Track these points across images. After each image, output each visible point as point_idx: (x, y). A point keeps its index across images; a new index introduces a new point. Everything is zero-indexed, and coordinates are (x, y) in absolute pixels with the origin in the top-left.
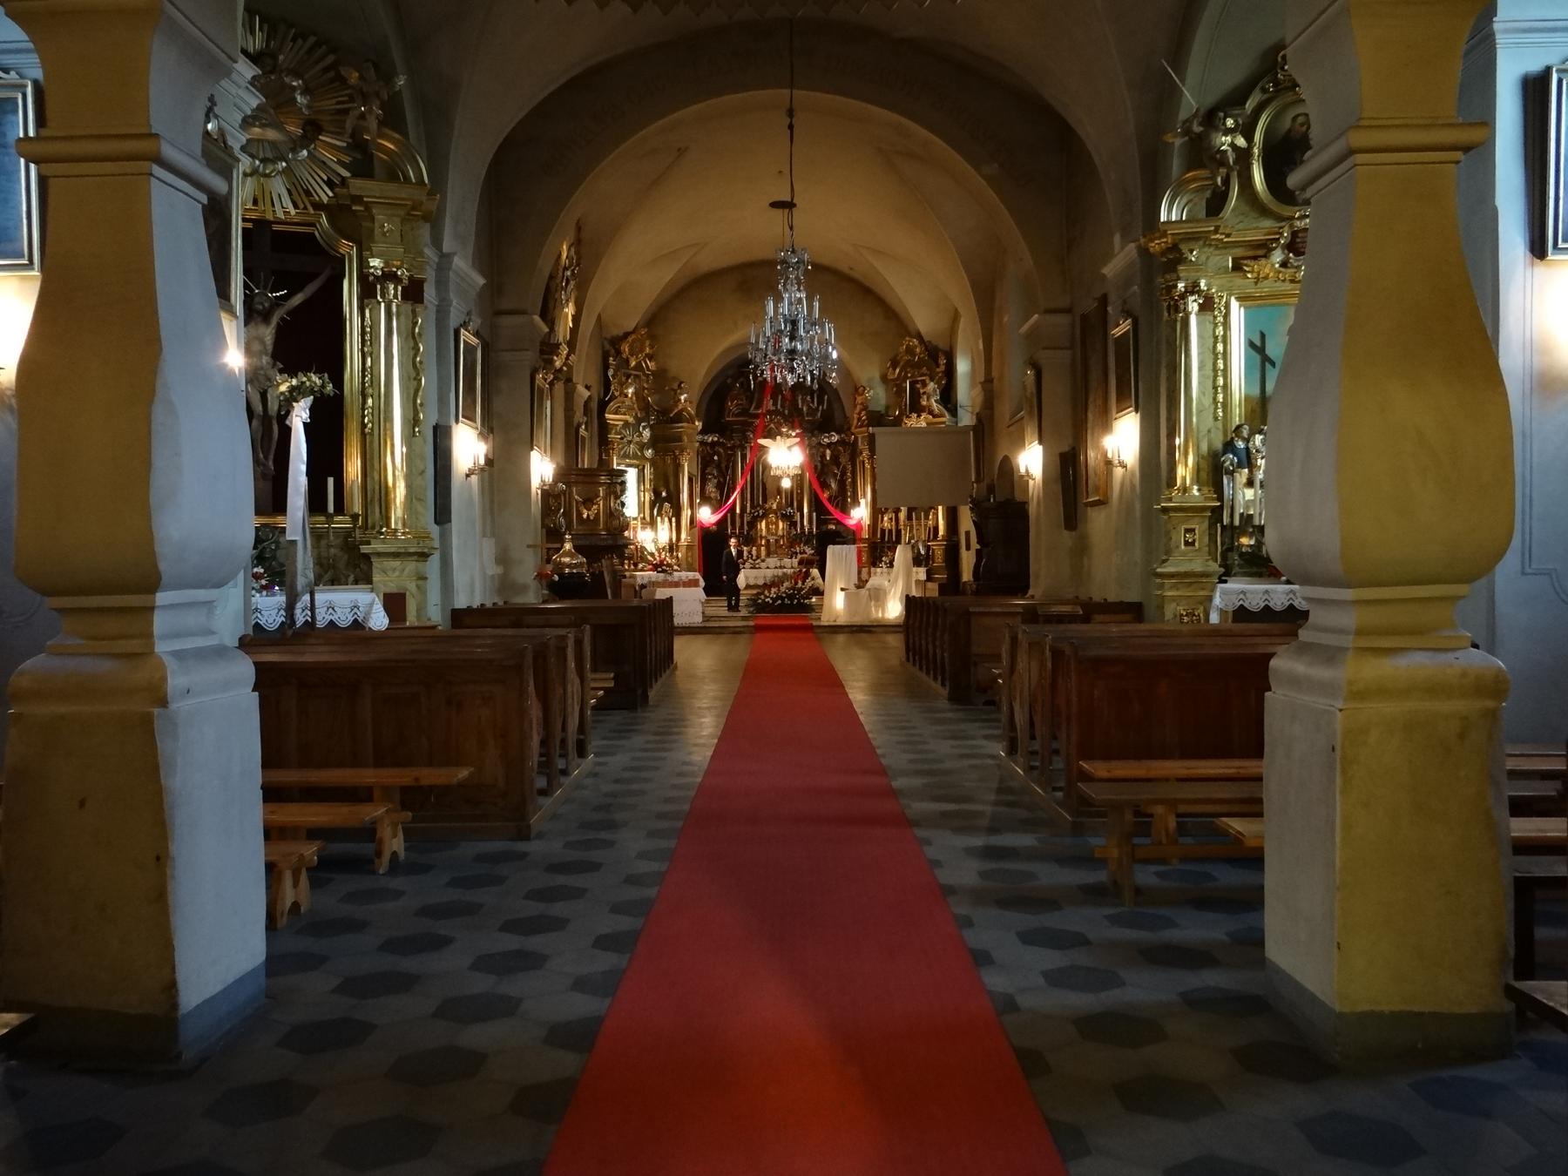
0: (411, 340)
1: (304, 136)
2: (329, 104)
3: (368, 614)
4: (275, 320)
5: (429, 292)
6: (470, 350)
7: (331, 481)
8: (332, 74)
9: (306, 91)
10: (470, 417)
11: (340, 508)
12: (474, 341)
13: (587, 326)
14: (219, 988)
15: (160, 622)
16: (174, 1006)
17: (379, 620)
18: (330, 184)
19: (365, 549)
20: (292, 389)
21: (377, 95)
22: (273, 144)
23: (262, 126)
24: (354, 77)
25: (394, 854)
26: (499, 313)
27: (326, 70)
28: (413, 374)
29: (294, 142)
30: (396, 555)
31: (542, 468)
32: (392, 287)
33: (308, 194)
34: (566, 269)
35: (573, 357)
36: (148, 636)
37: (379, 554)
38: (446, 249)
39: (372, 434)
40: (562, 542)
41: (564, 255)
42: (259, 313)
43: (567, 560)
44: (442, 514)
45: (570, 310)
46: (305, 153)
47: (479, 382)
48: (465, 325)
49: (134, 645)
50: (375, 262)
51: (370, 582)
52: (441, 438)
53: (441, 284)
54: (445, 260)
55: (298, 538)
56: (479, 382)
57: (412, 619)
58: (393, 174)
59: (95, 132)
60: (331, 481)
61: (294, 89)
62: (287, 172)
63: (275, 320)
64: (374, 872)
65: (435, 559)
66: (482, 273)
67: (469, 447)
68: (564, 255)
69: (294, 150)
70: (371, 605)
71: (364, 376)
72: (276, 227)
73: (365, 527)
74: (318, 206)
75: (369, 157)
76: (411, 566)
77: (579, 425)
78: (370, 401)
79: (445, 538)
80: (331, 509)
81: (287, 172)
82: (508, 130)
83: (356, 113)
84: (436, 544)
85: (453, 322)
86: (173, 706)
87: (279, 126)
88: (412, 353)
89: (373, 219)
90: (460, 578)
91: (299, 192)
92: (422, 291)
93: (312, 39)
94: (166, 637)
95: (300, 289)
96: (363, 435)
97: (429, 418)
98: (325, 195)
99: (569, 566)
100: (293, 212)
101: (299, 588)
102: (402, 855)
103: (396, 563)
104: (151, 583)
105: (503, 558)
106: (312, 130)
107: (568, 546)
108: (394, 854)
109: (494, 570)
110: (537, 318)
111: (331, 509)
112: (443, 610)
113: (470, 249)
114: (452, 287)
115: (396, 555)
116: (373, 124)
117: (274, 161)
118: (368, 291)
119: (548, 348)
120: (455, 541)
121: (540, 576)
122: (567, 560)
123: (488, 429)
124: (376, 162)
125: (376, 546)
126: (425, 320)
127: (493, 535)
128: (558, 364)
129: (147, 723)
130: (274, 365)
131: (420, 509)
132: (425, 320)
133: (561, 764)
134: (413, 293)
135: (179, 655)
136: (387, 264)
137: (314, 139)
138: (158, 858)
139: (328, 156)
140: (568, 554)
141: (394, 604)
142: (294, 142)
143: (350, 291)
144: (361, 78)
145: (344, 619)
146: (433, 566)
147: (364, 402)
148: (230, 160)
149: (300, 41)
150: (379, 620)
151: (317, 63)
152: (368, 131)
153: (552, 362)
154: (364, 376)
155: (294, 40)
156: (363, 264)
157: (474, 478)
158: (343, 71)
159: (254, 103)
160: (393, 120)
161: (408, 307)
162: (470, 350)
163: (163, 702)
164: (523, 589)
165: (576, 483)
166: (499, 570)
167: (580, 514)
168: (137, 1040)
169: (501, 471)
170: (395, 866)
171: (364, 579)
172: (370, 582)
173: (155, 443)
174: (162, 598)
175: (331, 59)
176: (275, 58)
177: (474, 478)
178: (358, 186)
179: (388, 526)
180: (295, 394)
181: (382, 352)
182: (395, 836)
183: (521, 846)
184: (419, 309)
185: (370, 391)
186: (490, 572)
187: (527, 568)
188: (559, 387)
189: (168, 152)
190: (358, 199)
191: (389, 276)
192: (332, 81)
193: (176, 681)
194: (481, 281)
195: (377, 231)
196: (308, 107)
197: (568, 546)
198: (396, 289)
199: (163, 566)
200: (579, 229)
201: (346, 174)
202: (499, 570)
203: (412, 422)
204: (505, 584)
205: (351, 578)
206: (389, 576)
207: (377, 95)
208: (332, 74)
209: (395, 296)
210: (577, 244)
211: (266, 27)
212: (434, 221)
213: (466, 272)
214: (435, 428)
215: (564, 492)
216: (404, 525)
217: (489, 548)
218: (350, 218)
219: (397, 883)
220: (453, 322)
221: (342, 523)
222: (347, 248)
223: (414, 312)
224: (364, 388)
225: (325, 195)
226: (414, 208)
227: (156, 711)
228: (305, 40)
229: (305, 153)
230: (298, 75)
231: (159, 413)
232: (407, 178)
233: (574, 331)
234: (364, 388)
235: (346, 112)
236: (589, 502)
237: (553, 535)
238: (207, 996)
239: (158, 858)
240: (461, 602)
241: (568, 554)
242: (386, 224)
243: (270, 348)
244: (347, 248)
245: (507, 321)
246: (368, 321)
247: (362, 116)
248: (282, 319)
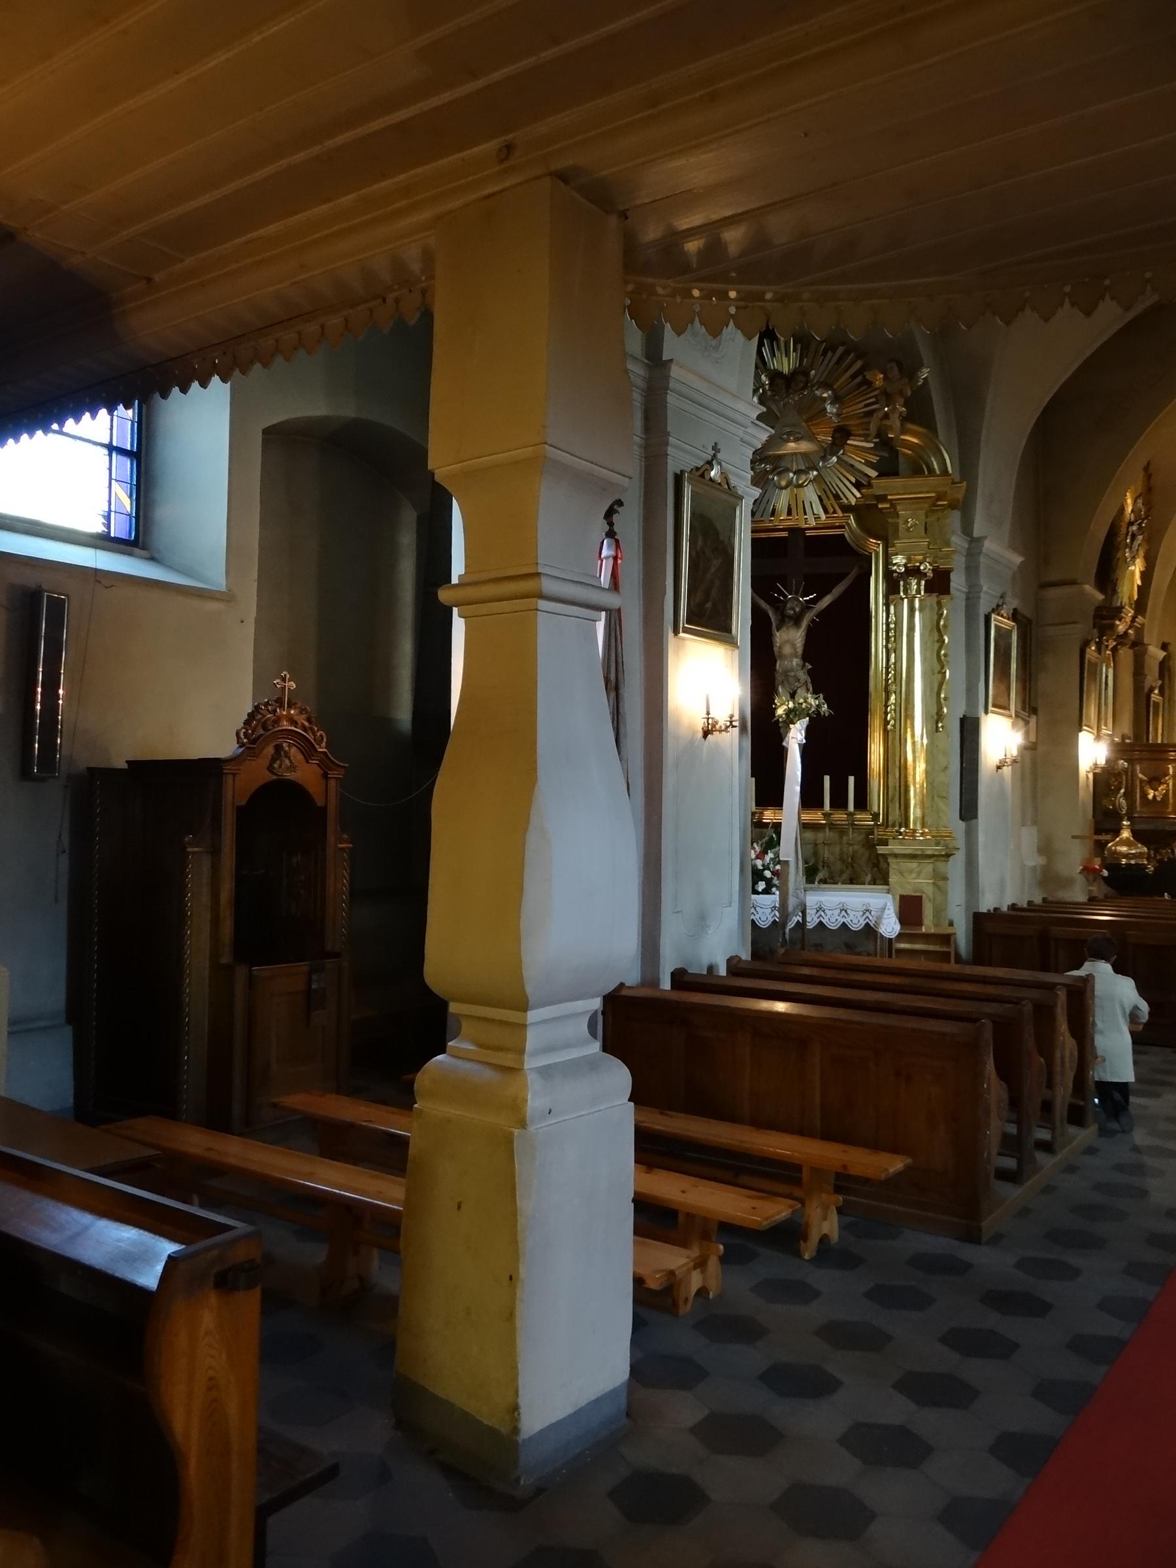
0: (936, 631)
1: (833, 444)
2: (859, 408)
3: (880, 918)
4: (805, 623)
5: (957, 581)
6: (1003, 635)
7: (851, 779)
8: (859, 379)
9: (836, 399)
10: (1002, 706)
11: (862, 802)
12: (1007, 624)
13: (1162, 579)
14: (570, 1410)
15: (532, 1039)
16: (516, 1430)
17: (890, 926)
18: (858, 485)
19: (881, 849)
20: (789, 712)
21: (901, 392)
22: (805, 455)
23: (796, 440)
24: (879, 379)
25: (824, 1239)
26: (1045, 586)
27: (854, 377)
28: (937, 667)
29: (825, 450)
30: (913, 857)
31: (1092, 751)
32: (914, 582)
33: (837, 497)
34: (1131, 524)
35: (1140, 619)
36: (521, 1051)
37: (896, 856)
38: (976, 533)
39: (894, 731)
40: (1117, 832)
41: (1129, 509)
42: (790, 617)
43: (1124, 849)
44: (969, 810)
45: (1137, 568)
46: (835, 459)
47: (1014, 666)
48: (997, 609)
49: (507, 1060)
50: (899, 560)
51: (886, 883)
52: (969, 731)
53: (972, 570)
54: (974, 544)
55: (791, 859)
56: (1014, 666)
57: (928, 925)
58: (918, 469)
59: (493, 575)
60: (851, 779)
61: (825, 399)
62: (819, 480)
63: (805, 623)
64: (798, 1254)
65: (959, 858)
66: (1020, 554)
67: (1001, 738)
68: (1129, 509)
69: (824, 459)
70: (883, 909)
71: (887, 673)
72: (809, 533)
73: (886, 824)
74: (846, 509)
75: (895, 454)
76: (928, 867)
77: (1151, 690)
78: (893, 698)
79: (971, 835)
80: (851, 807)
81: (819, 480)
82: (1055, 390)
83: (880, 414)
84: (960, 842)
85: (984, 607)
86: (532, 1129)
87: (811, 438)
88: (936, 646)
89: (898, 516)
90: (987, 876)
91: (830, 497)
92: (948, 580)
93: (841, 350)
94: (537, 1053)
95: (828, 592)
96: (886, 732)
97: (954, 712)
98: (853, 496)
99: (1126, 856)
100: (823, 517)
101: (790, 908)
102: (835, 1237)
103: (913, 865)
104: (523, 1006)
105: (1046, 848)
106: (842, 434)
107: (1126, 834)
108: (824, 1239)
109: (1035, 860)
110: (1089, 588)
111: (851, 807)
112: (967, 908)
113: (1007, 526)
114: (983, 571)
115: (913, 857)
116: (896, 422)
117: (806, 472)
118: (892, 587)
119: (1106, 615)
120: (981, 838)
121: (1087, 870)
122: (1124, 849)
123: (1029, 709)
124: (901, 459)
125: (894, 847)
126: (953, 608)
127: (1035, 822)
128: (1121, 627)
129: (509, 1140)
130: (804, 666)
131: (942, 805)
132: (953, 608)
133: (1043, 1135)
134: (939, 584)
135: (546, 1072)
136: (909, 560)
137: (843, 445)
138: (511, 1278)
139: (857, 461)
140: (1125, 842)
141: (910, 909)
142: (825, 450)
143: (877, 589)
144: (885, 378)
145: (856, 923)
146: (956, 868)
147: (888, 699)
148: (732, 499)
149: (830, 354)
150: (890, 926)
151: (846, 371)
152: (891, 428)
153: (1113, 627)
154: (887, 673)
155: (825, 353)
156: (887, 562)
157: (1007, 770)
158: (869, 376)
159: (764, 437)
160: (919, 412)
161: (933, 599)
162: (1003, 635)
163: (523, 1124)
164: (1068, 882)
165: (1140, 760)
166: (1041, 861)
167: (1144, 795)
168: (474, 1461)
169: (1045, 759)
170: (826, 1253)
171: (880, 878)
172: (886, 883)
173: (527, 871)
174: (532, 1016)
175: (859, 364)
176: (807, 374)
177: (1007, 770)
178: (882, 486)
179: (907, 826)
180: (793, 715)
181: (906, 643)
182: (825, 1218)
183: (969, 1253)
184: (945, 599)
185: (893, 688)
186: (1030, 863)
187: (1074, 857)
188: (1126, 654)
189: (548, 586)
190: (882, 498)
191: (913, 571)
192: (860, 385)
193: (535, 1101)
194: (1018, 559)
195: (902, 527)
196: (838, 415)
197: (1126, 834)
198: (919, 584)
199: (529, 989)
200: (1148, 477)
201: (873, 473)
202: (1041, 861)
203: (935, 719)
204: (1047, 877)
205: (869, 878)
206: (911, 878)
207: (901, 392)
208: (859, 379)
209: (918, 592)
210: (1147, 494)
211: (799, 346)
212: (965, 507)
213: (1000, 551)
214: (963, 721)
215: (1126, 771)
216: (923, 826)
217: (1029, 837)
218: (875, 518)
219: (820, 1278)
220: (984, 607)
221: (864, 819)
222: (876, 547)
223: (939, 604)
224: (887, 685)
225: (853, 496)
226: (939, 499)
227: (516, 1132)
228: (834, 352)
229: (835, 459)
230: (826, 385)
231: (532, 839)
232: (931, 471)
233: (1144, 590)
234: (887, 685)
235: (870, 414)
236: (1155, 780)
237: (1105, 821)
238: (554, 1420)
239: (511, 1278)
240: (987, 904)
241: (1125, 842)
242: (909, 519)
243: (800, 650)
244: (876, 547)
245: (1052, 593)
246: (892, 618)
247: (886, 416)
248: (813, 621)
